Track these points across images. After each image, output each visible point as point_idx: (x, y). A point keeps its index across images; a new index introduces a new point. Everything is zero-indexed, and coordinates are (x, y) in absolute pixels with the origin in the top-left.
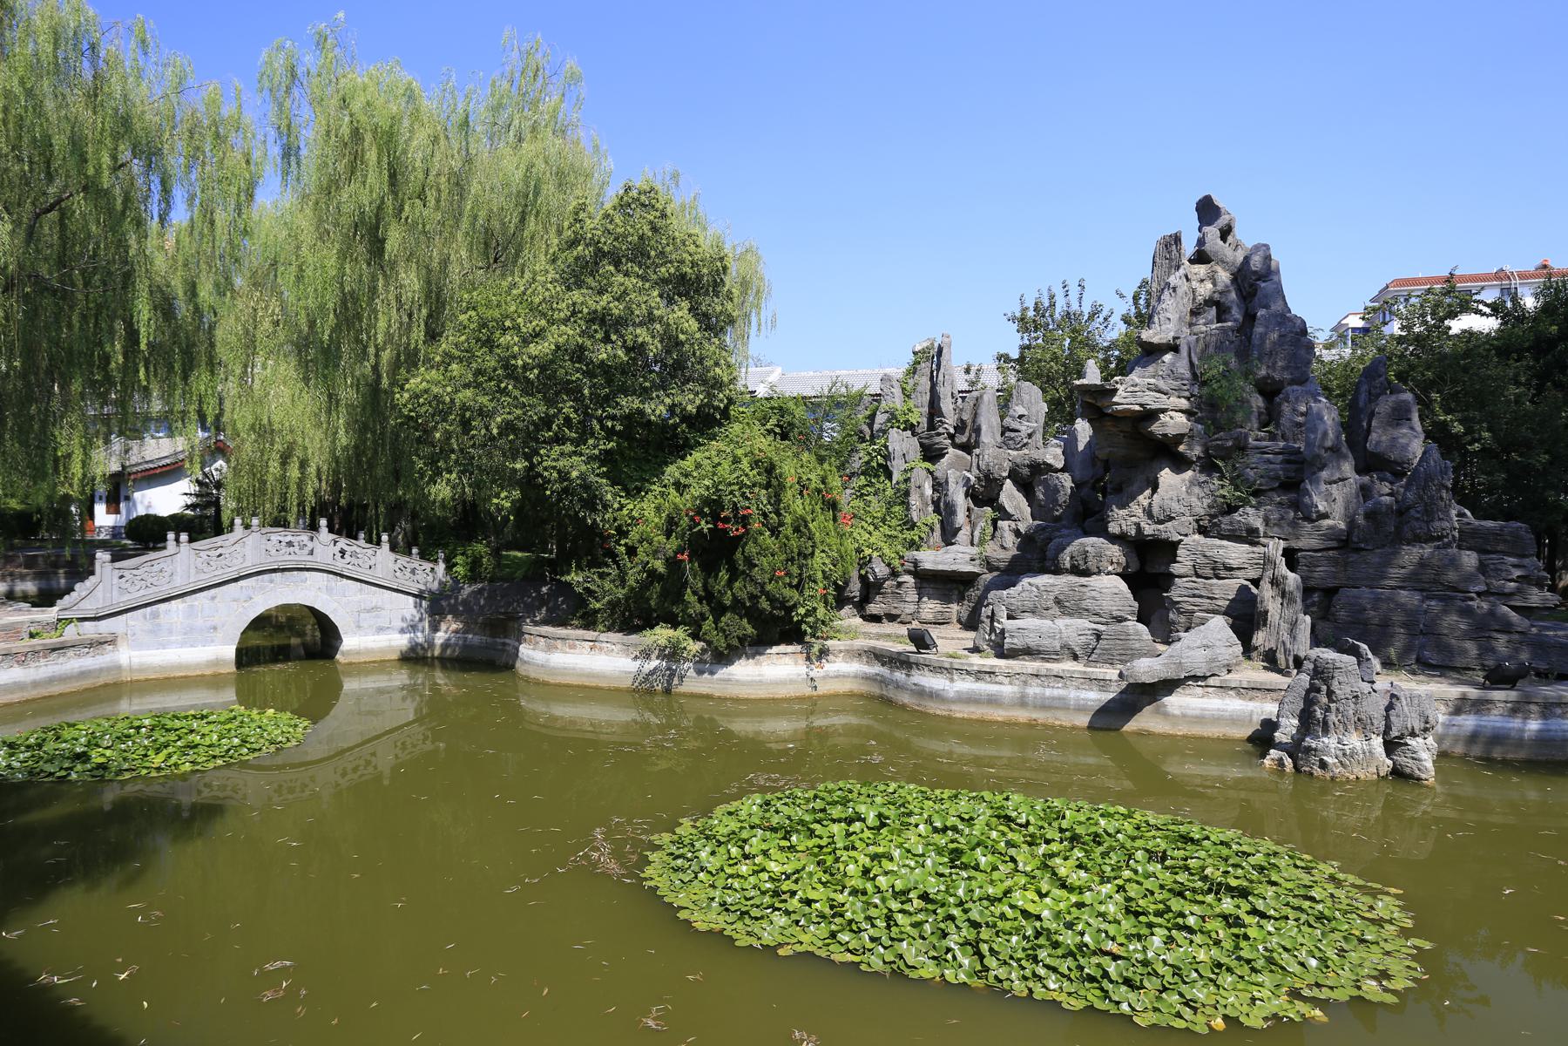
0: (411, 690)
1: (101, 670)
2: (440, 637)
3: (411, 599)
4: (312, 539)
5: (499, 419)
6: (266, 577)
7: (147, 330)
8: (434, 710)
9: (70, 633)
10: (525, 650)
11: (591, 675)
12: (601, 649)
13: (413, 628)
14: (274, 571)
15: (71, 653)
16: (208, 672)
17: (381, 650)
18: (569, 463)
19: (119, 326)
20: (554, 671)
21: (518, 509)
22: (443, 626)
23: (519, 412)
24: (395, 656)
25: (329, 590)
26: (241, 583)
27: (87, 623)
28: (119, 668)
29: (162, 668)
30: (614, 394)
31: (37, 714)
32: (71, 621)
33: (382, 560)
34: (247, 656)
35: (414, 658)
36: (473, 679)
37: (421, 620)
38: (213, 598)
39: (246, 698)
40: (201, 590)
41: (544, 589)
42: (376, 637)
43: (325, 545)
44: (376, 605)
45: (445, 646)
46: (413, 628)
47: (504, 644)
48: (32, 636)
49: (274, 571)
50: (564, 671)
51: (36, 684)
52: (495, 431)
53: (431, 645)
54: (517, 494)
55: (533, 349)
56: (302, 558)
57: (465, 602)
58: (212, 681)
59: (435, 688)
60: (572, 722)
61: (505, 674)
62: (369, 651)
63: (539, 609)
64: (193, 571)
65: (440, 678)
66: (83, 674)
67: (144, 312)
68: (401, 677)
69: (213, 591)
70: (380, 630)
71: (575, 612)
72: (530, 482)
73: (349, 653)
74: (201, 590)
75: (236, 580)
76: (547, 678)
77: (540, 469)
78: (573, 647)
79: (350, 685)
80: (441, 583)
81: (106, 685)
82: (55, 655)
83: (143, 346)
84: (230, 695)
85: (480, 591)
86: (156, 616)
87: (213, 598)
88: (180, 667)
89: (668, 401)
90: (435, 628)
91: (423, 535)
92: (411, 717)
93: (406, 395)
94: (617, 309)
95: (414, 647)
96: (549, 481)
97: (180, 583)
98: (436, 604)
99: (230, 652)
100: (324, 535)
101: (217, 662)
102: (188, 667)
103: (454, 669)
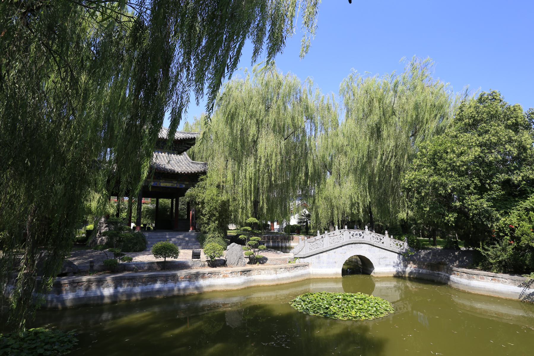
0: (398, 288)
1: (306, 274)
2: (408, 270)
3: (397, 255)
4: (363, 233)
5: (450, 186)
6: (350, 245)
7: (311, 170)
8: (407, 295)
9: (297, 262)
10: (453, 277)
11: (493, 292)
12: (499, 281)
13: (398, 265)
14: (352, 244)
15: (299, 268)
16: (334, 277)
17: (387, 273)
18: (477, 203)
19: (304, 168)
20: (473, 288)
21: (457, 220)
22: (409, 266)
23: (458, 183)
24: (392, 275)
25: (369, 250)
26: (343, 247)
27: (301, 259)
28: (310, 274)
29: (489, 291)
30: (494, 174)
31: (292, 287)
32: (297, 258)
33: (387, 240)
34: (344, 272)
35: (399, 276)
36: (426, 288)
37: (400, 263)
38: (335, 252)
39: (346, 288)
40: (331, 249)
41: (456, 253)
42: (386, 268)
43: (368, 235)
44: (385, 256)
45: (411, 273)
46: (398, 265)
47: (438, 274)
48: (289, 262)
49: (352, 244)
50: (479, 289)
51: (292, 278)
52: (450, 191)
53: (404, 272)
54: (456, 215)
55: (464, 158)
56: (360, 239)
57: (423, 257)
58: (335, 280)
59: (407, 287)
60: (486, 312)
61: (443, 287)
62: (384, 273)
63: (455, 261)
64: (329, 243)
65: (409, 284)
66: (302, 275)
67: (310, 164)
68: (393, 283)
69: (335, 250)
70: (387, 265)
71: (477, 262)
72: (462, 212)
73: (377, 273)
74: (331, 249)
75: (341, 246)
76: (469, 291)
77: (466, 205)
78: (483, 279)
79: (378, 285)
80: (406, 250)
81: (307, 279)
82: (295, 269)
83: (309, 174)
84: (340, 285)
85: (429, 253)
86: (319, 257)
87: (335, 252)
88: (326, 275)
89: (522, 174)
90: (406, 266)
91: (398, 230)
92: (399, 299)
93: (407, 181)
94: (494, 139)
95: (398, 273)
96: (470, 210)
97: (326, 247)
98: (406, 258)
99: (340, 271)
100: (367, 231)
101: (336, 274)
102: (328, 275)
103: (415, 282)
